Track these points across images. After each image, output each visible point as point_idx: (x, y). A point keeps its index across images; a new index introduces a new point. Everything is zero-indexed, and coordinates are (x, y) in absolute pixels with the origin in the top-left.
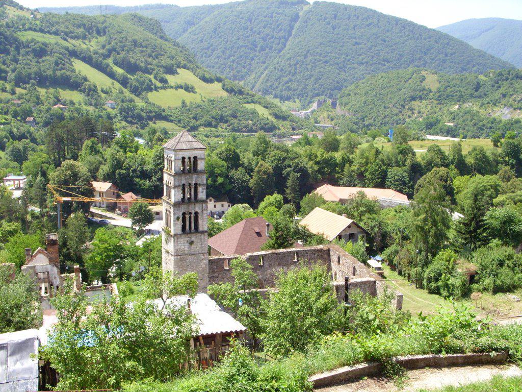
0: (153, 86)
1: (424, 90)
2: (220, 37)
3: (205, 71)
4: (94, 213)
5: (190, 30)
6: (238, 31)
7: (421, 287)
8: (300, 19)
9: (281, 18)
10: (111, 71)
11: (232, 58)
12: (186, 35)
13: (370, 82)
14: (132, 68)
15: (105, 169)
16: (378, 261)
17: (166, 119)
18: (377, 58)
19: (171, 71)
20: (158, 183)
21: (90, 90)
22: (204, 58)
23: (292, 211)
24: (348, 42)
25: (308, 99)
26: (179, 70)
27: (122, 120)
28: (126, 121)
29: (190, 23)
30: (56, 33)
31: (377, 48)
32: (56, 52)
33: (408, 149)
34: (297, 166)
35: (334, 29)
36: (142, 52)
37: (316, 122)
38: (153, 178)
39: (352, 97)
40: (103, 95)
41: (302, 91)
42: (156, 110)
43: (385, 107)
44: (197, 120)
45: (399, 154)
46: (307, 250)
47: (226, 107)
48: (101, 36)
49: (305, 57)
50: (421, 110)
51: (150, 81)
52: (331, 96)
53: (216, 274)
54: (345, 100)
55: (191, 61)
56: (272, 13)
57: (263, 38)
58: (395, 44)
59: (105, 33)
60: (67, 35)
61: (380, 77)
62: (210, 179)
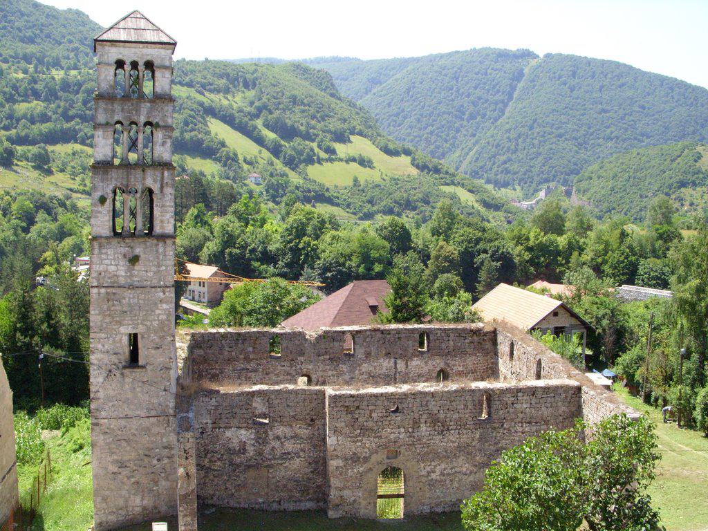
0: (315, 158)
1: (699, 172)
2: (414, 100)
3: (389, 141)
4: (188, 309)
5: (374, 91)
6: (440, 93)
7: (690, 424)
8: (524, 78)
9: (498, 76)
10: (258, 134)
11: (430, 128)
12: (369, 96)
13: (621, 161)
14: (288, 133)
15: (212, 247)
16: (607, 377)
17: (330, 201)
18: (632, 131)
19: (341, 138)
20: (285, 270)
21: (228, 158)
22: (392, 128)
23: (455, 285)
24: (591, 109)
25: (534, 185)
26: (352, 138)
27: (268, 200)
28: (274, 202)
29: (375, 82)
30: (190, 85)
31: (631, 118)
32: (187, 108)
33: (672, 233)
34: (497, 251)
35: (572, 90)
36: (303, 111)
38: (280, 262)
39: (595, 181)
40: (246, 167)
41: (525, 174)
42: (317, 188)
43: (641, 196)
44: (373, 205)
45: (658, 239)
46: (449, 329)
47: (415, 189)
48: (249, 90)
49: (531, 128)
50: (695, 201)
51: (312, 150)
52: (565, 182)
53: (253, 365)
54: (584, 185)
55: (370, 127)
56: (487, 70)
57: (473, 103)
58: (658, 112)
59: (254, 85)
60: (204, 87)
61: (635, 155)
62: (362, 266)
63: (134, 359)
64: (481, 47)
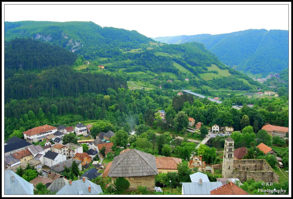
17: (207, 85)
19: (209, 65)
37: (268, 85)
63: (229, 169)
64: (248, 29)
